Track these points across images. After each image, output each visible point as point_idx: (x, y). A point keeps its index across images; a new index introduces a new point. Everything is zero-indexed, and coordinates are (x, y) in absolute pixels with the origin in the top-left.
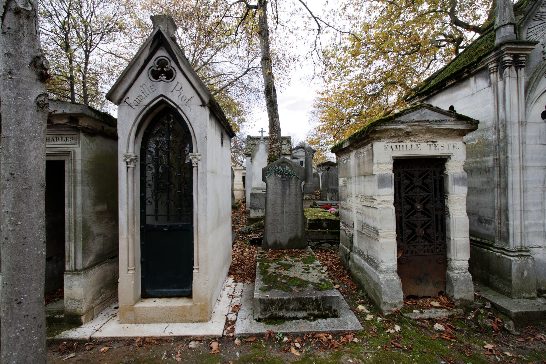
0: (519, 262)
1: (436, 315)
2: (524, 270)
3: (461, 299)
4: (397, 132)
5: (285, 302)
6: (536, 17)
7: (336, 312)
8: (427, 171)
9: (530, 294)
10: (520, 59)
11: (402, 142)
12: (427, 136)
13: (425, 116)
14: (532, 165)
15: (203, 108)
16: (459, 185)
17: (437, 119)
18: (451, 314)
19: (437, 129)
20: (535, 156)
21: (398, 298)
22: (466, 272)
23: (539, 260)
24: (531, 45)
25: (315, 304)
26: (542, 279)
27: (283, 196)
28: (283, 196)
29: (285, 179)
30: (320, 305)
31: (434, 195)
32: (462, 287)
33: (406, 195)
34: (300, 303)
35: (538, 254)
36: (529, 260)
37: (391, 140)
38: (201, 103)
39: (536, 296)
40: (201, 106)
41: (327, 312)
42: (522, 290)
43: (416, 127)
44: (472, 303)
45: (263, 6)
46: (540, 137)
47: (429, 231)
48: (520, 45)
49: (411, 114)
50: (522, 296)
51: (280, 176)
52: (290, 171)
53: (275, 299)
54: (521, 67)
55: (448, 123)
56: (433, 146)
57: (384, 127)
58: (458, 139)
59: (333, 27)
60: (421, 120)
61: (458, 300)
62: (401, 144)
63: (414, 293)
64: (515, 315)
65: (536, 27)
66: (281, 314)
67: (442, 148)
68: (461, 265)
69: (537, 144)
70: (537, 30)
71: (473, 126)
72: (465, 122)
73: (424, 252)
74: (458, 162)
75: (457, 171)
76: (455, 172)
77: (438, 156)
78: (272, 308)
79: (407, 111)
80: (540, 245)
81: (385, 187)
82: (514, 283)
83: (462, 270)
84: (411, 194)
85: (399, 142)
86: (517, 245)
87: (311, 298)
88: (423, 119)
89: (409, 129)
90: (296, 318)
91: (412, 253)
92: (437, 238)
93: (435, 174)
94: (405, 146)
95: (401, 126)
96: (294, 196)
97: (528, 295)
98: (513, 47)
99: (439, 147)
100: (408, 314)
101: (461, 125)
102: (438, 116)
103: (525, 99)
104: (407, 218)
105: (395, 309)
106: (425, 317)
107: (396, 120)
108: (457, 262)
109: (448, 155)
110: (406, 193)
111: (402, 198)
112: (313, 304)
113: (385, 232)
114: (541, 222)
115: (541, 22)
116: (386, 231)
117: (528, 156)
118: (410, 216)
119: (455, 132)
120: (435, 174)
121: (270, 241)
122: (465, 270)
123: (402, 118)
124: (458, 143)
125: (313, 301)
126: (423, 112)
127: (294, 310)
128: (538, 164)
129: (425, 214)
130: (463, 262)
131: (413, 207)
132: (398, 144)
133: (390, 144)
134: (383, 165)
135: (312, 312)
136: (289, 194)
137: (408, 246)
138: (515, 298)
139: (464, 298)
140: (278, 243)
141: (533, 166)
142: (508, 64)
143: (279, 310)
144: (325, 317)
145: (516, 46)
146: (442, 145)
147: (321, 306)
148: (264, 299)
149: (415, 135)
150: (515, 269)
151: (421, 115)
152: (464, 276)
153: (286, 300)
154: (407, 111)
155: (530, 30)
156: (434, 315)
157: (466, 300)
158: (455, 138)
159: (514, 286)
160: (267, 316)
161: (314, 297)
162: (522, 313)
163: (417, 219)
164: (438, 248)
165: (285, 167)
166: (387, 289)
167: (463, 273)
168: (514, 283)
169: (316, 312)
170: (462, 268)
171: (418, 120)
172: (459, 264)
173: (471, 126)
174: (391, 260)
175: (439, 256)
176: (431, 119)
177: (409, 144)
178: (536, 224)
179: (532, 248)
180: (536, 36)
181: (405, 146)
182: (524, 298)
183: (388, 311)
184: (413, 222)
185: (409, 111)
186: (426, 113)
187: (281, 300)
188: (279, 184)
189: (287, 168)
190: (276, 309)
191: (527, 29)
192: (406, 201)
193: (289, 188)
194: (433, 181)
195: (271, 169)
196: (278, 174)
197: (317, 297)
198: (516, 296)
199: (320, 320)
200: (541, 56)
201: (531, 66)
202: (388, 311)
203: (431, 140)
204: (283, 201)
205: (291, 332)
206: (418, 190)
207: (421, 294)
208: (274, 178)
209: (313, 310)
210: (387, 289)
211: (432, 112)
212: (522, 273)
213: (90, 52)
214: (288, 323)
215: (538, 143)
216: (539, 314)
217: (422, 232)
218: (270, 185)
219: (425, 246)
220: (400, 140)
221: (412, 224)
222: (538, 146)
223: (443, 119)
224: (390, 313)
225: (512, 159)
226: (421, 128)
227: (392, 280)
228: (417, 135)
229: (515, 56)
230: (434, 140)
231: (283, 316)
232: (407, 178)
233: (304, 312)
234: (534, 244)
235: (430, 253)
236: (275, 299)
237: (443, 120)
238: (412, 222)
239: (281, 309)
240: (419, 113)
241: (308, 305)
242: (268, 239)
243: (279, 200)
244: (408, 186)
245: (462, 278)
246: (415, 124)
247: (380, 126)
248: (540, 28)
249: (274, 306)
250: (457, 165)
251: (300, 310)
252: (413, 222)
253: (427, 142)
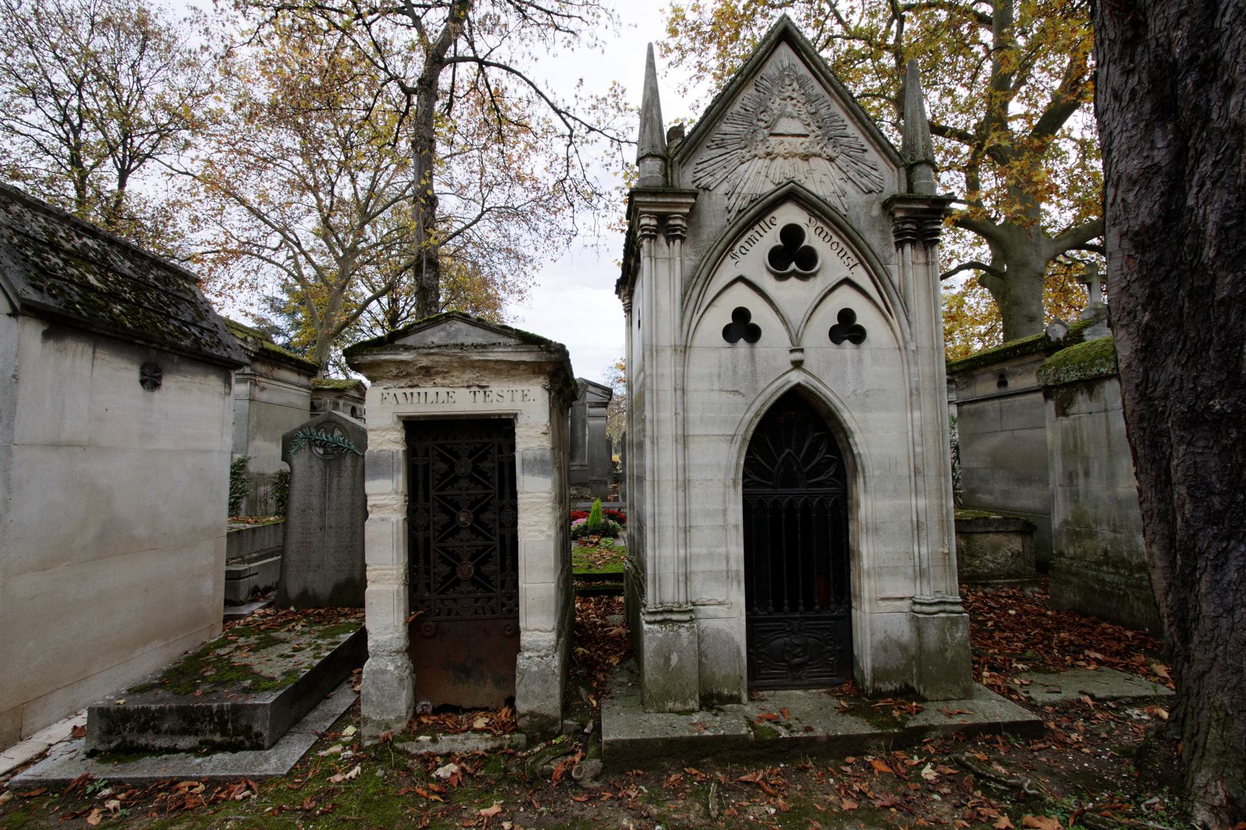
0: (660, 635)
1: (465, 748)
2: (670, 652)
3: (532, 714)
4: (402, 368)
5: (153, 715)
6: (713, 141)
7: (260, 738)
8: (485, 444)
9: (684, 702)
10: (671, 222)
11: (417, 386)
12: (468, 376)
13: (455, 336)
14: (703, 433)
15: (13, 320)
16: (534, 475)
17: (480, 340)
18: (497, 744)
19: (479, 360)
20: (710, 415)
21: (394, 710)
22: (547, 656)
23: (719, 631)
24: (685, 197)
25: (216, 720)
26: (723, 672)
27: (324, 494)
28: (325, 492)
29: (332, 457)
30: (227, 722)
31: (497, 493)
32: (533, 687)
33: (439, 493)
34: (184, 718)
35: (716, 617)
36: (682, 630)
37: (395, 383)
38: (9, 310)
39: (697, 708)
40: (9, 315)
41: (241, 738)
42: (666, 695)
43: (436, 358)
44: (554, 722)
45: (425, 89)
46: (719, 376)
47: (485, 569)
48: (663, 197)
49: (428, 331)
50: (667, 709)
51: (321, 451)
52: (341, 439)
53: (132, 709)
54: (674, 238)
55: (500, 349)
56: (480, 395)
57: (370, 358)
58: (535, 381)
59: (601, 132)
60: (447, 343)
61: (524, 715)
62: (415, 390)
63: (452, 700)
64: (607, 747)
65: (711, 162)
66: (142, 741)
67: (499, 398)
68: (535, 641)
69: (712, 390)
70: (714, 167)
71: (553, 356)
72: (535, 348)
73: (476, 612)
74: (533, 427)
75: (532, 445)
76: (526, 447)
77: (494, 415)
78: (124, 730)
79: (417, 327)
80: (720, 599)
81: (378, 478)
82: (649, 680)
83: (538, 651)
84: (449, 492)
85: (411, 387)
86: (666, 600)
87: (210, 708)
88: (453, 342)
89: (425, 362)
90: (173, 750)
91: (449, 614)
92: (503, 582)
93: (500, 452)
94: (422, 395)
95: (405, 356)
96: (348, 492)
97: (679, 706)
98: (648, 200)
99: (494, 396)
100: (405, 744)
101: (526, 354)
102: (483, 336)
103: (682, 304)
104: (442, 541)
105: (383, 734)
106: (441, 750)
107: (396, 343)
108: (528, 633)
109: (512, 414)
110: (442, 489)
111: (431, 499)
112: (211, 720)
113: (375, 570)
114: (723, 550)
115: (723, 151)
116: (378, 567)
117: (693, 415)
118: (447, 537)
119: (522, 367)
120: (500, 452)
121: (294, 589)
122: (544, 651)
123: (410, 340)
124: (531, 388)
125: (211, 713)
126: (453, 329)
127: (172, 732)
128: (716, 431)
129: (479, 534)
130: (540, 633)
131: (453, 518)
132: (408, 391)
133: (392, 392)
134: (379, 432)
135: (208, 737)
136: (339, 489)
137: (442, 600)
138: (651, 711)
139: (537, 711)
140: (311, 592)
141: (706, 435)
142: (679, 233)
143: (139, 732)
144: (234, 748)
145: (654, 199)
146: (501, 393)
147: (230, 724)
148: (108, 709)
149: (445, 374)
150: (651, 649)
151: (449, 334)
152: (538, 665)
153: (156, 710)
154: (417, 327)
155: (700, 167)
156: (460, 747)
157: (542, 716)
158: (528, 379)
159: (648, 686)
160: (113, 745)
161: (215, 705)
162: (623, 742)
163: (462, 544)
164: (504, 605)
165: (333, 433)
166: (372, 691)
167: (539, 657)
168: (649, 680)
169: (218, 738)
170: (538, 646)
171: (440, 343)
172: (531, 639)
173: (548, 356)
174: (386, 628)
175: (506, 622)
176: (469, 341)
177: (432, 391)
178: (711, 556)
179: (704, 605)
180: (711, 178)
181: (422, 395)
182: (671, 711)
183: (371, 737)
184: (453, 551)
185: (422, 325)
186: (458, 330)
187: (145, 711)
188: (317, 466)
189: (337, 433)
190: (132, 730)
191: (694, 165)
192: (440, 506)
193: (339, 476)
194: (496, 465)
195: (301, 435)
196: (316, 445)
197: (222, 707)
198: (652, 707)
199: (219, 756)
200: (724, 216)
201: (705, 237)
202: (371, 737)
203: (477, 383)
204: (324, 502)
205: (130, 779)
206: (464, 483)
207: (467, 703)
208: (307, 454)
209: (212, 732)
210: (372, 691)
211: (472, 328)
212: (668, 659)
213: (129, 171)
214: (148, 761)
215: (715, 388)
216: (660, 744)
217: (470, 571)
218: (298, 469)
219: (477, 600)
220: (415, 382)
221: (452, 554)
222: (715, 395)
223: (494, 341)
224: (376, 742)
225: (652, 421)
226: (447, 359)
227: (384, 672)
228: (446, 372)
229: (662, 218)
230: (484, 384)
231: (147, 745)
232: (444, 459)
233: (192, 737)
234: (705, 597)
235: (488, 615)
236: (132, 709)
237: (494, 344)
238: (450, 550)
239: (142, 730)
240: (444, 329)
241: (202, 723)
242: (288, 585)
243: (316, 502)
244: (444, 476)
245: (535, 669)
246: (432, 351)
247: (362, 355)
248: (721, 163)
249: (128, 725)
250: (531, 434)
251: (184, 732)
252: (453, 551)
253: (468, 387)
